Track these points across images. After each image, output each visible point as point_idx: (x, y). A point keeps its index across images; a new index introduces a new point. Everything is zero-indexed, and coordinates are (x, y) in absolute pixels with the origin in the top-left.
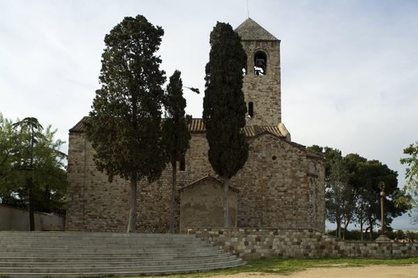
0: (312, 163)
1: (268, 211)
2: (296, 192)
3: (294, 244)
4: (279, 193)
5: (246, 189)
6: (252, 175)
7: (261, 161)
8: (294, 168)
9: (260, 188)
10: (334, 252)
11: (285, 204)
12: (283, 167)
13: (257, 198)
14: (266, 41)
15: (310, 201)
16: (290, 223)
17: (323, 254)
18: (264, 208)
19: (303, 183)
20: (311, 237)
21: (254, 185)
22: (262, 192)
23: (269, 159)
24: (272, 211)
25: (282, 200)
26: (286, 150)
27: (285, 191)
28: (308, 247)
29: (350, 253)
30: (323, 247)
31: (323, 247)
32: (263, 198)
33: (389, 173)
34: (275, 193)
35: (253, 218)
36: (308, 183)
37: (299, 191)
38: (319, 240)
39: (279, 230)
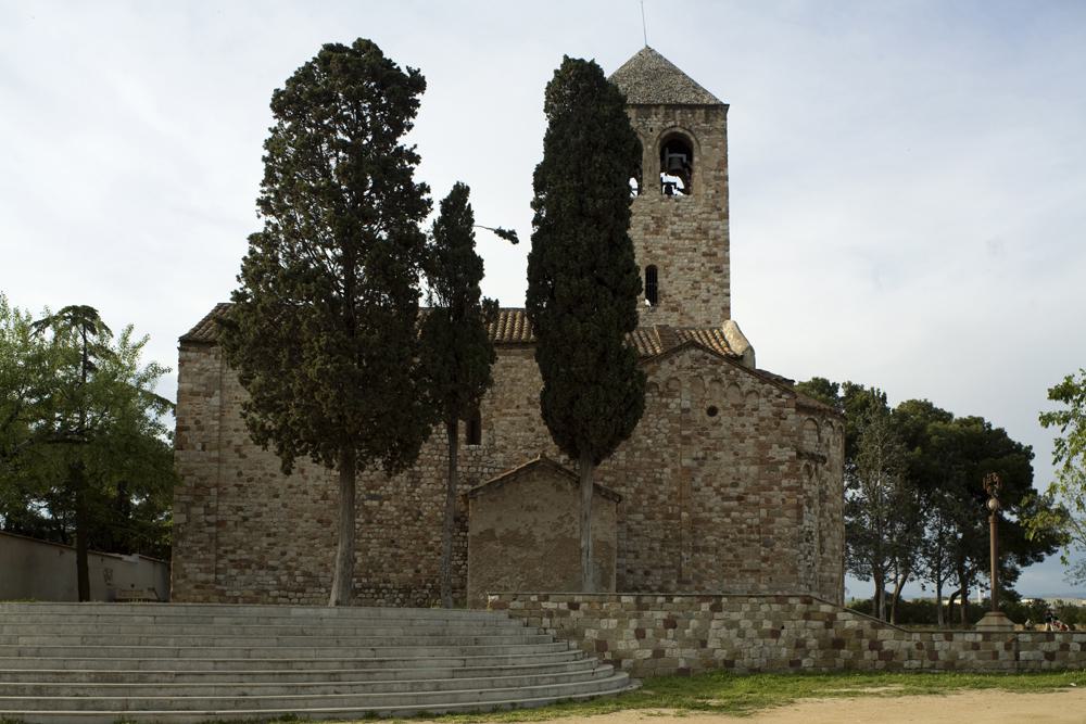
0: (810, 425)
1: (696, 549)
2: (768, 501)
3: (762, 635)
4: (726, 503)
5: (639, 491)
6: (654, 455)
7: (679, 420)
8: (762, 438)
9: (675, 489)
10: (868, 655)
11: (741, 531)
12: (737, 435)
13: (669, 517)
14: (692, 107)
17: (840, 662)
18: (684, 543)
19: (786, 475)
20: (807, 616)
21: (660, 482)
23: (699, 415)
24: (705, 549)
25: (734, 521)
26: (744, 389)
27: (740, 498)
28: (800, 644)
30: (838, 644)
31: (838, 644)
35: (654, 567)
36: (799, 478)
37: (777, 496)
38: (828, 625)
39: (724, 600)
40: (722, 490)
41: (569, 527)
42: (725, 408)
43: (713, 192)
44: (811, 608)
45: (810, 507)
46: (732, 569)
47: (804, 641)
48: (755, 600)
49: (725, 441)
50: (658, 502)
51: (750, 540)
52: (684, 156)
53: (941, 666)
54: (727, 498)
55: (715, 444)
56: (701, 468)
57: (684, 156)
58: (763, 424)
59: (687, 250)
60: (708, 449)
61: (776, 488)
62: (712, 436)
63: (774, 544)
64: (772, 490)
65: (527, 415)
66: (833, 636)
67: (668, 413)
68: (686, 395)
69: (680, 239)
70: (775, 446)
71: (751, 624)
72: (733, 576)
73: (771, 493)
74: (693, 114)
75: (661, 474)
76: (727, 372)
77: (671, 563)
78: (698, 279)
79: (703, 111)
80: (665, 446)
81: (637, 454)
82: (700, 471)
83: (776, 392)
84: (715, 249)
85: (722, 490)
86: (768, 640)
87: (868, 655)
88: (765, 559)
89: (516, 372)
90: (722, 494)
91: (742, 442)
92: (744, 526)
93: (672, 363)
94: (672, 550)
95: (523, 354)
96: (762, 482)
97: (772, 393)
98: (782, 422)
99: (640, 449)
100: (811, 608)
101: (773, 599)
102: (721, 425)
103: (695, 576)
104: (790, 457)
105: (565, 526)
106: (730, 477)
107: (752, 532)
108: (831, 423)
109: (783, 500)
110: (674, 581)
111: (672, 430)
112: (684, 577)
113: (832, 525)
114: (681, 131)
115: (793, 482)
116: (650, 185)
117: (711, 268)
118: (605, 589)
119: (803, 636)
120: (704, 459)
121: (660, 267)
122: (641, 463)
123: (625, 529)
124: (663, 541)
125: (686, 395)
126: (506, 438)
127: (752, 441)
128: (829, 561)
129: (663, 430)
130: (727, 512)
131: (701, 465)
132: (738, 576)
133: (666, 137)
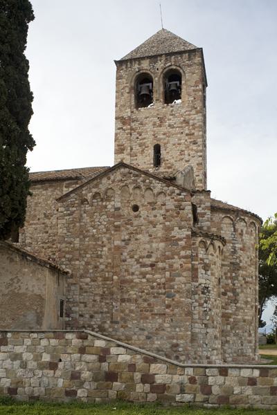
0: (227, 221)
1: (123, 300)
2: (171, 266)
3: (42, 366)
4: (143, 269)
5: (87, 263)
6: (98, 239)
7: (113, 216)
8: (167, 223)
9: (110, 261)
10: (139, 388)
11: (152, 288)
12: (151, 222)
13: (106, 279)
14: (181, 53)
15: (201, 281)
16: (160, 321)
17: (112, 394)
18: (115, 296)
19: (184, 248)
20: (82, 350)
21: (100, 256)
22: (113, 267)
23: (127, 211)
24: (129, 300)
25: (148, 280)
26: (156, 191)
27: (152, 265)
28: (75, 376)
29: (182, 391)
30: (111, 376)
31: (111, 376)
32: (115, 277)
33: (19, 123)
34: (135, 268)
35: (96, 313)
36: (196, 249)
37: (177, 263)
38: (102, 359)
39: (9, 335)
40: (141, 260)
41: (17, 285)
42: (143, 205)
43: (193, 99)
44: (86, 343)
45: (206, 270)
46: (147, 313)
47: (79, 373)
48: (35, 335)
49: (143, 227)
50: (99, 270)
51: (159, 294)
52: (178, 83)
53: (214, 401)
54: (144, 265)
55: (136, 230)
56: (127, 246)
57: (178, 83)
58: (168, 214)
59: (177, 134)
60: (132, 233)
61: (176, 257)
62: (134, 225)
63: (174, 296)
64: (173, 258)
65: (43, 224)
66: (106, 369)
67: (106, 212)
68: (117, 199)
69: (173, 127)
70: (176, 228)
71: (32, 356)
72: (147, 318)
73: (173, 261)
74: (181, 57)
75: (101, 251)
76: (144, 181)
77: (107, 310)
78: (184, 149)
79: (187, 54)
80: (105, 233)
81: (87, 239)
82: (126, 248)
83: (177, 191)
84: (193, 131)
85: (141, 260)
86: (46, 371)
87: (139, 388)
88: (168, 306)
89: (38, 199)
90: (141, 263)
91: (154, 227)
92: (155, 284)
93: (109, 179)
94: (107, 301)
95: (42, 188)
96: (167, 253)
97: (174, 192)
98: (181, 212)
99: (89, 236)
100: (86, 343)
101: (52, 335)
102: (140, 217)
103: (122, 319)
104: (187, 235)
105: (15, 284)
106: (146, 251)
107: (160, 288)
108: (244, 220)
109: (181, 265)
110: (108, 322)
111: (109, 222)
112: (114, 319)
113: (245, 286)
114: (174, 67)
115: (189, 252)
116: (157, 100)
117: (191, 142)
118: (39, 327)
119: (77, 368)
120: (129, 240)
121: (162, 145)
122: (89, 245)
123: (78, 288)
124: (102, 295)
125: (117, 199)
126: (31, 238)
127: (161, 226)
128: (242, 308)
129: (103, 223)
130: (144, 275)
131: (127, 244)
132: (150, 318)
133: (166, 72)
